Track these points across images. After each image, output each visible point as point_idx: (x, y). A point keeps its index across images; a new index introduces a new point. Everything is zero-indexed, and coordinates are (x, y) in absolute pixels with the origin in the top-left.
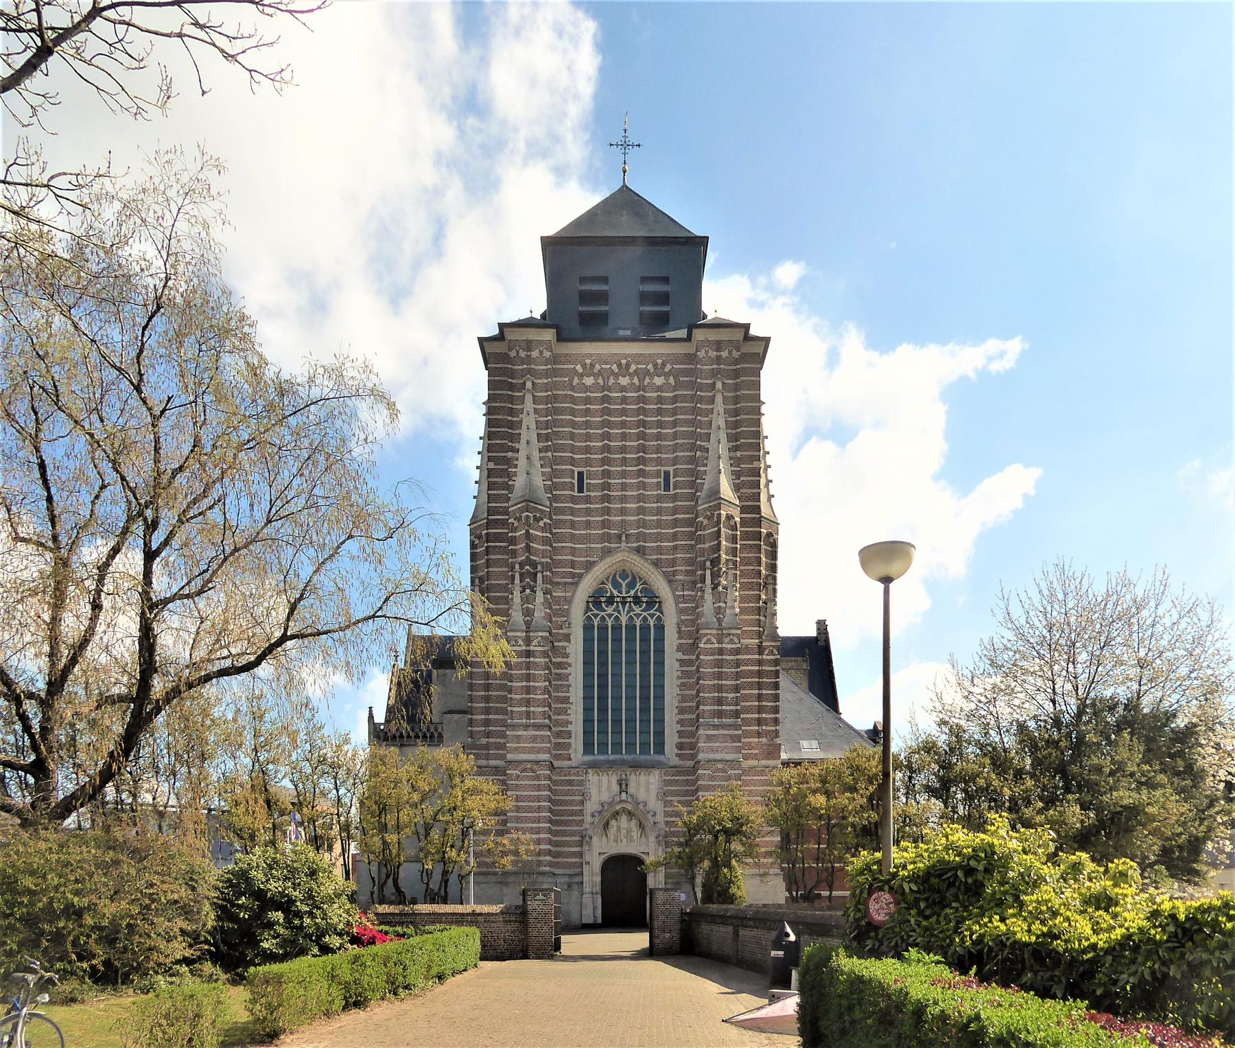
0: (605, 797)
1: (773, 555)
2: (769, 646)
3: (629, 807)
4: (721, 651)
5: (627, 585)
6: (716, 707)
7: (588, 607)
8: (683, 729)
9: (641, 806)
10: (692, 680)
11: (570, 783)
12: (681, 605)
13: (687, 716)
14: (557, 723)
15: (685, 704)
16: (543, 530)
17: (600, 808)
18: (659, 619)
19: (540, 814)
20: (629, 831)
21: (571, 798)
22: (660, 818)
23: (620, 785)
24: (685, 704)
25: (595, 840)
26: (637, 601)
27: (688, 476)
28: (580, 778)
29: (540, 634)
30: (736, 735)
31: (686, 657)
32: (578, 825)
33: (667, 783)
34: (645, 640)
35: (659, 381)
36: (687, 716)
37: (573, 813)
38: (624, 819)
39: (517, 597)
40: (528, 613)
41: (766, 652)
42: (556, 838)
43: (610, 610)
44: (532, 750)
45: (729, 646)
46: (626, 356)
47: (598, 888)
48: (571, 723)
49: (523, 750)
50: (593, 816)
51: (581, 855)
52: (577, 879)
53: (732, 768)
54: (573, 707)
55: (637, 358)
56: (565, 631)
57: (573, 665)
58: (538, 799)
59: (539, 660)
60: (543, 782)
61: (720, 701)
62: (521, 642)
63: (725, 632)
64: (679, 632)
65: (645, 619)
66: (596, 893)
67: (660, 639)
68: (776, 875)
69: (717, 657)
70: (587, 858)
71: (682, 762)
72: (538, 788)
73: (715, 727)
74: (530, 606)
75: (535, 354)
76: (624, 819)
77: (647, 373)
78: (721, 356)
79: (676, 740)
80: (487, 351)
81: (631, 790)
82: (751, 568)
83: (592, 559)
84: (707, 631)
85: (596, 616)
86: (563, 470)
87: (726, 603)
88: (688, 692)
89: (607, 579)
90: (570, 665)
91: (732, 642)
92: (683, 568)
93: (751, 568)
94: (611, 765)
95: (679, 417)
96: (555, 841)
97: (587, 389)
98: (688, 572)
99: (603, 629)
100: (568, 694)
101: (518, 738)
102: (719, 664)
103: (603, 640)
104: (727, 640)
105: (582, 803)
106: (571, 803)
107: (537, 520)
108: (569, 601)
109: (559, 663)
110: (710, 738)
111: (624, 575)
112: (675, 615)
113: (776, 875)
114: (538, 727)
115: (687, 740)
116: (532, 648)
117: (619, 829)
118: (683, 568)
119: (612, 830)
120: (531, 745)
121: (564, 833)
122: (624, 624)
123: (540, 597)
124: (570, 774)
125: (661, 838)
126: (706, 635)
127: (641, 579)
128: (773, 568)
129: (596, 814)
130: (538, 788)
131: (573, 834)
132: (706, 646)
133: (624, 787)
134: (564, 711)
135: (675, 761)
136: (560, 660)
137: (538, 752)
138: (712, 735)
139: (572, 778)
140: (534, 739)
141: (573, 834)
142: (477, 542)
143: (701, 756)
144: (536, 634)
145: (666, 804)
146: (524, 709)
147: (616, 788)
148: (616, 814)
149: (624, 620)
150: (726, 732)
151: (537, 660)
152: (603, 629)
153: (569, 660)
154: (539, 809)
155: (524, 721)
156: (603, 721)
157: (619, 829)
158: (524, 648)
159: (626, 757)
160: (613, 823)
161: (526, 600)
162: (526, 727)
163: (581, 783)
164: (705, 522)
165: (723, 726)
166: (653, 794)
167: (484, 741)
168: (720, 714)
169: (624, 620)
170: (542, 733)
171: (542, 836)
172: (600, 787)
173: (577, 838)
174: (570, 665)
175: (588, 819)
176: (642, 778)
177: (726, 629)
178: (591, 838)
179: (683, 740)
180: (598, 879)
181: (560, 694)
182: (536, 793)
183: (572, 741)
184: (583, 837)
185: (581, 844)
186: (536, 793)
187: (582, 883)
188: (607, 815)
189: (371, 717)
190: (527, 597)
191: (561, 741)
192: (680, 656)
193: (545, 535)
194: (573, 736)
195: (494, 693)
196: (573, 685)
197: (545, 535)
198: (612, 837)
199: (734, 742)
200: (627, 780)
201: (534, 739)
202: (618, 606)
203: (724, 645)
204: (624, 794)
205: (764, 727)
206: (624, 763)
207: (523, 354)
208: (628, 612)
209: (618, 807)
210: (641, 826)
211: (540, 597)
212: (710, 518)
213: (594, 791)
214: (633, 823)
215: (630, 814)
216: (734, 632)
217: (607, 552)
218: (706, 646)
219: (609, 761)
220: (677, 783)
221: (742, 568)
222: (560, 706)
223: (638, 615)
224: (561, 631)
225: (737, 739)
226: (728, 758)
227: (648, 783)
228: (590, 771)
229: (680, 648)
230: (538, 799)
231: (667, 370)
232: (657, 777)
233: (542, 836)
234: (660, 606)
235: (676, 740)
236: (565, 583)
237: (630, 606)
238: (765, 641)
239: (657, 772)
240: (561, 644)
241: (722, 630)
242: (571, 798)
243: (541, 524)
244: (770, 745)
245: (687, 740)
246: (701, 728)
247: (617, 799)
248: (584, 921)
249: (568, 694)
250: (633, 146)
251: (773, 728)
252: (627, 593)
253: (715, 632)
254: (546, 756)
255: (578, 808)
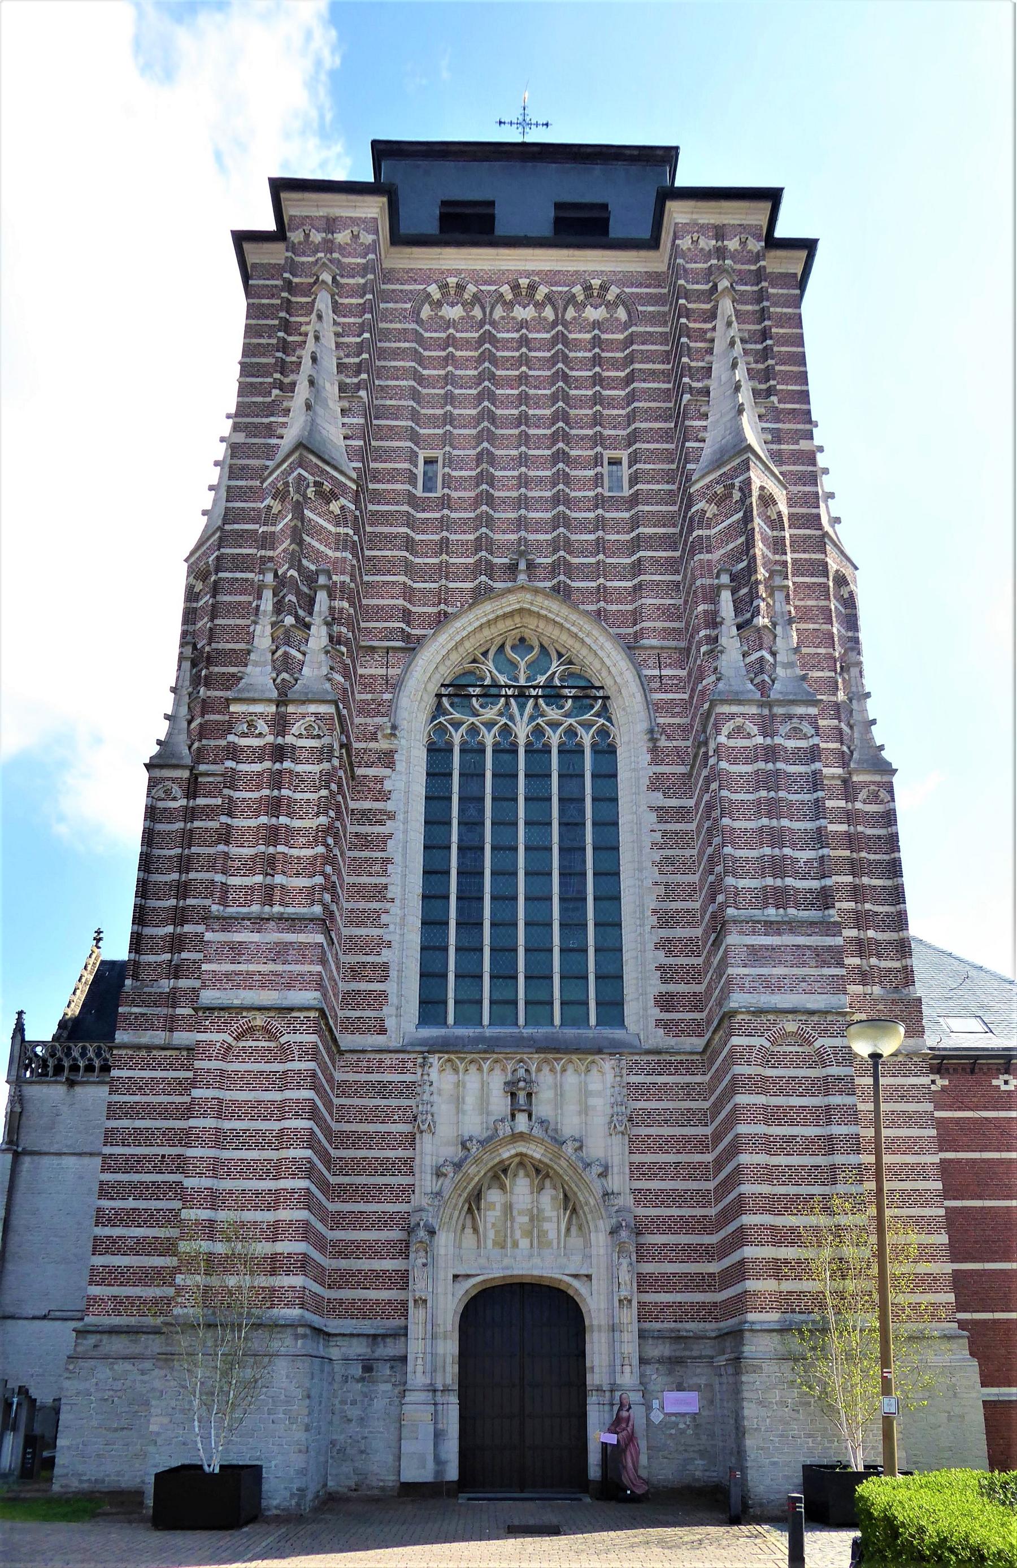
0: (473, 1125)
1: (851, 622)
2: (866, 784)
3: (536, 1152)
4: (771, 753)
5: (529, 666)
6: (769, 881)
7: (439, 705)
8: (671, 961)
9: (569, 1149)
10: (688, 853)
11: (382, 1090)
12: (657, 696)
13: (679, 932)
14: (354, 945)
15: (674, 905)
16: (339, 520)
17: (458, 1153)
18: (603, 732)
19: (284, 1153)
20: (536, 1218)
21: (382, 1128)
22: (619, 1181)
23: (513, 1095)
24: (674, 905)
25: (444, 1240)
26: (553, 695)
27: (663, 462)
28: (408, 1078)
29: (312, 708)
30: (830, 948)
31: (674, 802)
32: (397, 1199)
33: (637, 1091)
34: (571, 776)
35: (592, 314)
36: (679, 932)
37: (387, 1167)
38: (521, 1187)
39: (263, 637)
40: (285, 664)
41: (863, 795)
42: (339, 1235)
43: (490, 713)
44: (267, 982)
45: (791, 744)
46: (528, 274)
47: (450, 1374)
48: (389, 945)
49: (247, 981)
50: (439, 1174)
51: (402, 1280)
52: (390, 1349)
53: (825, 1033)
54: (395, 909)
55: (552, 277)
56: (383, 745)
57: (400, 817)
58: (282, 1111)
59: (308, 768)
60: (296, 1065)
61: (778, 867)
62: (262, 726)
63: (779, 710)
64: (654, 750)
65: (571, 732)
66: (446, 1390)
67: (607, 775)
68: (948, 1338)
69: (761, 765)
70: (419, 1286)
71: (671, 1042)
72: (283, 1081)
73: (771, 927)
74: (293, 652)
75: (342, 237)
76: (521, 1187)
77: (571, 299)
78: (725, 248)
79: (656, 986)
80: (251, 259)
81: (543, 1108)
82: (811, 626)
83: (450, 610)
84: (734, 709)
85: (457, 725)
86: (394, 450)
87: (774, 654)
88: (679, 878)
89: (485, 654)
90: (391, 816)
91: (796, 733)
92: (659, 625)
93: (811, 626)
94: (490, 1046)
95: (637, 366)
96: (334, 1244)
97: (449, 324)
98: (668, 613)
99: (473, 751)
100: (383, 880)
101: (236, 951)
102: (771, 781)
103: (472, 775)
104: (784, 729)
105: (411, 1141)
106: (384, 1140)
107: (328, 497)
108: (395, 685)
109: (364, 813)
110: (756, 955)
111: (522, 644)
112: (643, 714)
113: (948, 1338)
114: (292, 923)
115: (682, 988)
116: (289, 739)
117: (508, 1208)
118: (659, 625)
119: (491, 1215)
120: (271, 967)
121: (357, 1221)
122: (522, 741)
123: (318, 637)
124: (380, 1068)
125: (624, 1234)
126: (732, 716)
127: (560, 655)
128: (854, 644)
129: (449, 1170)
130: (283, 1081)
131: (384, 1221)
132: (732, 743)
133: (522, 1096)
134: (374, 918)
135: (658, 1038)
136: (367, 805)
137: (289, 986)
138: (767, 948)
139: (387, 1077)
140: (279, 952)
141: (384, 1221)
142: (199, 586)
143: (737, 1000)
144: (301, 709)
145: (636, 1145)
146: (259, 879)
147: (500, 1104)
148: (499, 1174)
149: (522, 732)
150: (801, 940)
151: (299, 768)
152: (473, 751)
153: (390, 806)
154: (282, 1139)
155: (255, 908)
156: (470, 949)
157: (508, 1208)
158: (270, 739)
159: (527, 1031)
160: (493, 1196)
161: (283, 638)
162: (259, 922)
163: (409, 1089)
164: (711, 510)
165: (793, 926)
166: (599, 1121)
167: (166, 985)
168: (781, 898)
169: (522, 732)
170: (302, 938)
171: (284, 1214)
172: (458, 1101)
173: (396, 1235)
174: (391, 816)
175: (425, 1182)
176: (571, 1079)
177: (781, 703)
178: (432, 1233)
179: (672, 988)
180: (450, 1348)
181: (365, 880)
182: (278, 1096)
183: (390, 986)
184: (410, 1230)
185: (403, 1250)
186: (278, 1096)
187: (404, 1359)
188: (476, 1172)
189: (20, 1029)
190: (287, 632)
191: (363, 986)
192: (658, 799)
193: (342, 530)
194: (393, 974)
195: (199, 876)
196: (398, 859)
197: (342, 530)
198: (491, 1234)
199: (825, 964)
200: (529, 1082)
201: (279, 952)
202: (507, 704)
203: (778, 740)
204: (522, 1118)
205: (873, 961)
206: (520, 1043)
207: (317, 237)
208: (532, 718)
209: (506, 1153)
210: (569, 1204)
211: (318, 637)
212: (719, 501)
213: (443, 1110)
214: (548, 1200)
215: (541, 1173)
216: (800, 710)
217: (481, 595)
218: (732, 743)
219: (480, 1039)
220: (662, 1091)
221: (798, 603)
222: (362, 905)
223: (554, 725)
224: (372, 745)
225: (834, 956)
226: (811, 1006)
227: (585, 1093)
228: (434, 1059)
229: (657, 783)
230: (282, 1111)
231: (610, 297)
232: (610, 1077)
233: (284, 1214)
234: (605, 707)
235: (656, 986)
236: (388, 649)
237: (536, 705)
238: (857, 771)
239: (608, 1065)
240: (371, 772)
241: (770, 705)
242: (382, 1128)
243: (335, 507)
244: (894, 1002)
245: (682, 988)
246: (732, 928)
247: (505, 1130)
248: (412, 1473)
249: (383, 880)
250: (537, 125)
251: (897, 965)
252: (528, 679)
253: (754, 710)
254: (309, 997)
255: (400, 1153)
